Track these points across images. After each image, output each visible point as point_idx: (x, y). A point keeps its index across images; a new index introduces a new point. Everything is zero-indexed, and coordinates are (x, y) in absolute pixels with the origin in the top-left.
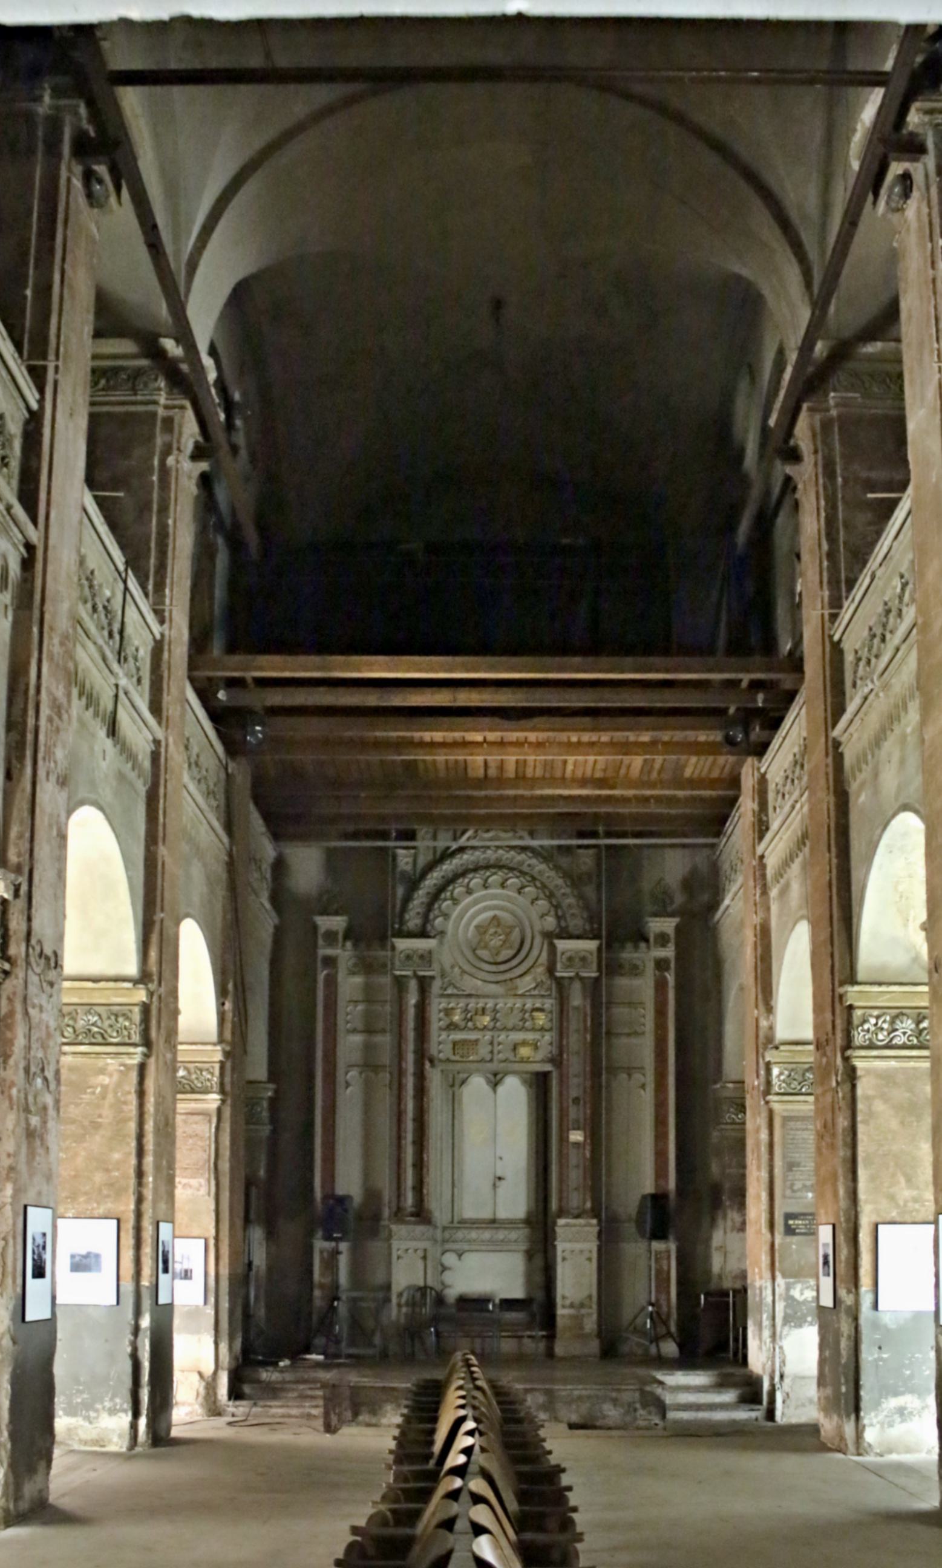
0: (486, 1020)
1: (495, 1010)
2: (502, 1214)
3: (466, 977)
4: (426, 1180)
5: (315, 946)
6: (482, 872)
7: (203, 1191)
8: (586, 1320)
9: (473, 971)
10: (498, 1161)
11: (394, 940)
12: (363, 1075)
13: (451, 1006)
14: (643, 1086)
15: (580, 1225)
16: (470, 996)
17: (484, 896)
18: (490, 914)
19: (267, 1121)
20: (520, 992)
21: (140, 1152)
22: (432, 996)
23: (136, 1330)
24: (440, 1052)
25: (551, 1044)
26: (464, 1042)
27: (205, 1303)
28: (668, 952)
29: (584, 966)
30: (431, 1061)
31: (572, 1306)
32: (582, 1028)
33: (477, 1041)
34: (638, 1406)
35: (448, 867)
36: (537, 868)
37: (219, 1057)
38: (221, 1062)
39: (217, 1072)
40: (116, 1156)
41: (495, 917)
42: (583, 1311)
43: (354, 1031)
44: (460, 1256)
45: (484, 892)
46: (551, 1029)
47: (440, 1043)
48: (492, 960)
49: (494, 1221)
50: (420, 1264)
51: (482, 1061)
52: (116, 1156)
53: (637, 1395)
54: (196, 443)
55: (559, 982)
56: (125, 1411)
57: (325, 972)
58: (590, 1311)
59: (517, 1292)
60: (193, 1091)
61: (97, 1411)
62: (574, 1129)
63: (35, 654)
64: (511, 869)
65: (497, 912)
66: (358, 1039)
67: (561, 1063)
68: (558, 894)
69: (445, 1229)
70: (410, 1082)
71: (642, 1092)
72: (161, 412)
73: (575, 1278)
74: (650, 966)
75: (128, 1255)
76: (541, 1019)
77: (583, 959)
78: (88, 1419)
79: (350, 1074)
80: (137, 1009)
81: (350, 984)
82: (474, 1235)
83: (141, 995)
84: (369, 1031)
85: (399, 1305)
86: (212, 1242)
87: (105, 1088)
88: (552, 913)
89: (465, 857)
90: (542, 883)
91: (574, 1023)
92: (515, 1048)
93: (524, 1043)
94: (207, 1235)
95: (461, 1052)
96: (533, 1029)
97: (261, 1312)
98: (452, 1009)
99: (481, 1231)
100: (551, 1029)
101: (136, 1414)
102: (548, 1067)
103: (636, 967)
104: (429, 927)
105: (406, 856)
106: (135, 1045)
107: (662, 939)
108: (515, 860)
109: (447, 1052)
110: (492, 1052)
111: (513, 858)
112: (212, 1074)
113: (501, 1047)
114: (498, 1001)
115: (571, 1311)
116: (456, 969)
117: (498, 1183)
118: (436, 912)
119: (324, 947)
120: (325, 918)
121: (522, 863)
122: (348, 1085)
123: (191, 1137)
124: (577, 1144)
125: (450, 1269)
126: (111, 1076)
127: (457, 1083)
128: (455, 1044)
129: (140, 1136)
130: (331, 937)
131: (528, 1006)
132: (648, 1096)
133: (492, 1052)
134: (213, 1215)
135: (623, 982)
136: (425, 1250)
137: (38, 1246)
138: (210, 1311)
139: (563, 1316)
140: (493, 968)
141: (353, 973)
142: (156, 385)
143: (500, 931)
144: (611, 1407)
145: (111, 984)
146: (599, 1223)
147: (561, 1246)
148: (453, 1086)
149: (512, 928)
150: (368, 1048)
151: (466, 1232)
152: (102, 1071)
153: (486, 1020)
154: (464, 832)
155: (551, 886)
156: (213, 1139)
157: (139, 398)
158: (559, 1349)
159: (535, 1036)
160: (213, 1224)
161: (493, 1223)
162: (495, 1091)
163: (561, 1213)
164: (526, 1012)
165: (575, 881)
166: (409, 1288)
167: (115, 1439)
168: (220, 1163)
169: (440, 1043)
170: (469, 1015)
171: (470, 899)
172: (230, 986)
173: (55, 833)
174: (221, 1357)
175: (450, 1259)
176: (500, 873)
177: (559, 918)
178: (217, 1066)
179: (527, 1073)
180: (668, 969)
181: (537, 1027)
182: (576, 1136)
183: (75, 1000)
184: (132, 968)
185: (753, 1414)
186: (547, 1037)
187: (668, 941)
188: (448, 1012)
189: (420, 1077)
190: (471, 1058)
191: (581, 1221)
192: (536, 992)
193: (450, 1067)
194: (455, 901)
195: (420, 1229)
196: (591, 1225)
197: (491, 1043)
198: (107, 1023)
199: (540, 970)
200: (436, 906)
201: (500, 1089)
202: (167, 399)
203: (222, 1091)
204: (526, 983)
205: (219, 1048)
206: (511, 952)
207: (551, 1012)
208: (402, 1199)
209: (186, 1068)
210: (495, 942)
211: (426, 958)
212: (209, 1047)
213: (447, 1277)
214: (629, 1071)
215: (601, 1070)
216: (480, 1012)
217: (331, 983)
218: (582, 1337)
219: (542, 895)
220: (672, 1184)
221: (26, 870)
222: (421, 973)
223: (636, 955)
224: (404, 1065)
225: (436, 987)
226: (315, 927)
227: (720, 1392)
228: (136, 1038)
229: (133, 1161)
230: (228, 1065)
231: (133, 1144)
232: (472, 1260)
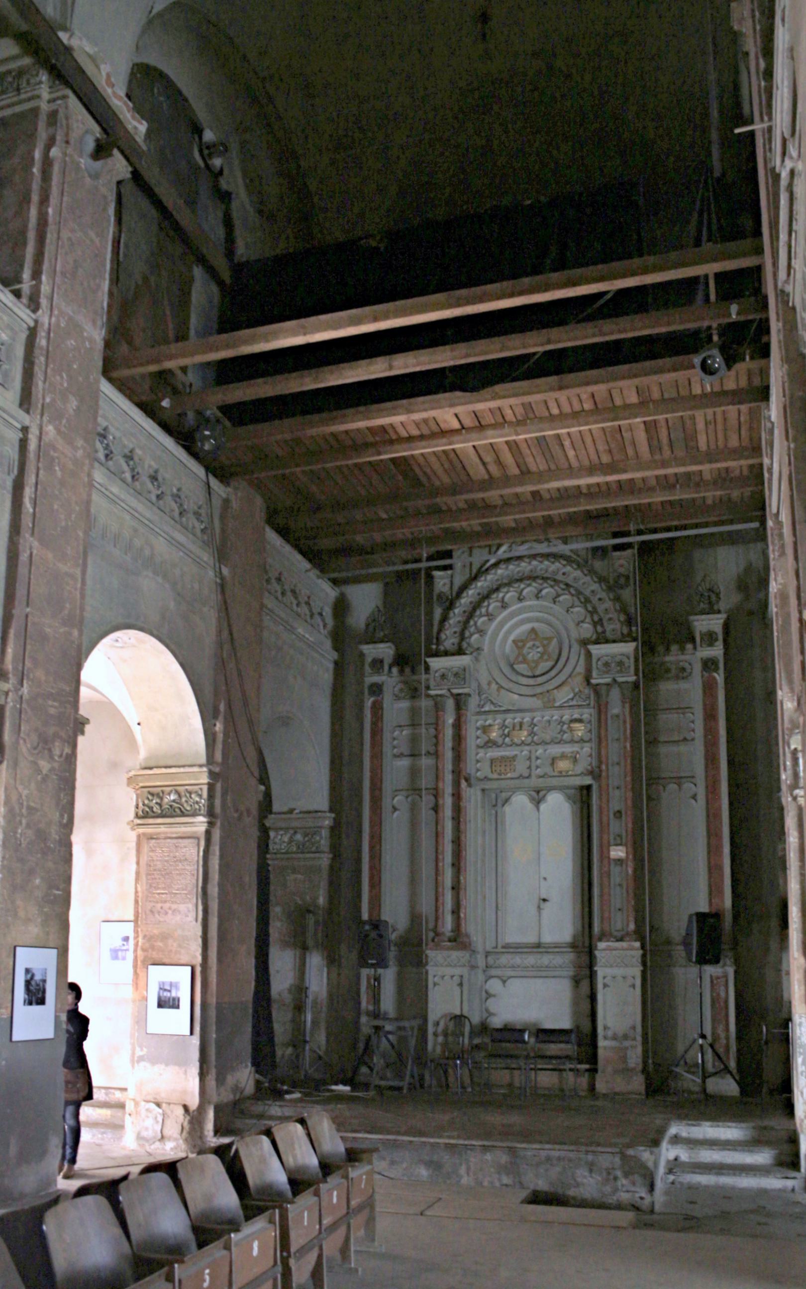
0: (524, 735)
1: (533, 724)
2: (547, 939)
3: (503, 691)
4: (463, 903)
5: (363, 675)
6: (516, 585)
8: (629, 1053)
9: (511, 685)
10: (543, 882)
11: (428, 660)
12: (410, 799)
13: (487, 723)
14: (694, 797)
15: (623, 949)
16: (508, 711)
17: (520, 608)
18: (527, 627)
19: (327, 849)
20: (557, 704)
22: (469, 714)
24: (478, 770)
25: (591, 756)
26: (503, 759)
27: (192, 1033)
28: (717, 651)
29: (621, 671)
30: (467, 780)
31: (615, 1038)
32: (622, 737)
33: (514, 758)
34: (619, 1173)
35: (482, 584)
36: (572, 576)
37: (205, 779)
38: (209, 784)
39: (205, 794)
41: (533, 630)
42: (627, 1044)
43: (401, 755)
44: (504, 982)
45: (519, 605)
46: (590, 741)
47: (478, 761)
48: (530, 674)
49: (538, 945)
50: (457, 990)
51: (521, 777)
53: (617, 1160)
54: (97, 140)
55: (596, 689)
57: (372, 699)
58: (634, 1043)
59: (565, 1023)
60: (183, 815)
62: (617, 845)
64: (545, 579)
65: (536, 625)
66: (405, 762)
67: (600, 776)
68: (595, 600)
69: (487, 954)
70: (448, 802)
71: (693, 801)
72: (45, 107)
73: (619, 1008)
74: (698, 667)
76: (580, 730)
77: (620, 664)
79: (396, 799)
81: (396, 709)
82: (518, 960)
84: (414, 755)
85: (435, 1034)
86: (198, 970)
88: (588, 619)
89: (500, 572)
90: (576, 590)
91: (613, 731)
92: (553, 761)
93: (563, 756)
94: (194, 962)
95: (498, 769)
96: (572, 741)
97: (321, 1039)
98: (490, 725)
99: (524, 956)
100: (590, 741)
102: (588, 781)
103: (683, 669)
104: (464, 645)
105: (442, 578)
107: (710, 638)
108: (551, 569)
109: (485, 771)
110: (529, 768)
111: (548, 567)
112: (200, 796)
113: (539, 761)
114: (535, 714)
115: (613, 1043)
116: (494, 686)
117: (543, 905)
118: (472, 629)
119: (371, 675)
120: (371, 646)
121: (555, 573)
122: (395, 809)
123: (180, 861)
124: (619, 861)
125: (494, 996)
127: (500, 803)
128: (492, 761)
130: (377, 664)
131: (566, 718)
132: (699, 808)
133: (529, 768)
134: (200, 941)
135: (666, 687)
136: (462, 976)
138: (196, 1041)
139: (605, 1048)
140: (531, 681)
141: (397, 698)
142: (38, 79)
143: (537, 643)
144: (586, 1174)
146: (643, 947)
147: (601, 972)
148: (495, 806)
149: (550, 639)
150: (414, 773)
151: (509, 956)
153: (524, 735)
154: (499, 546)
155: (587, 593)
156: (201, 863)
157: (23, 96)
158: (601, 1086)
159: (576, 748)
160: (200, 950)
161: (538, 947)
162: (538, 809)
163: (603, 936)
164: (564, 723)
165: (613, 585)
166: (445, 1016)
168: (209, 887)
169: (478, 761)
170: (506, 731)
171: (505, 613)
172: (222, 707)
175: (494, 985)
176: (534, 584)
177: (595, 624)
178: (205, 788)
179: (568, 787)
180: (716, 669)
181: (576, 738)
182: (618, 853)
185: (790, 1183)
186: (587, 749)
187: (716, 640)
188: (486, 729)
189: (457, 796)
190: (509, 775)
191: (624, 944)
192: (574, 703)
193: (487, 785)
194: (491, 617)
195: (455, 954)
196: (632, 949)
197: (529, 759)
199: (579, 680)
200: (472, 623)
201: (543, 807)
202: (50, 93)
203: (211, 813)
204: (563, 696)
205: (205, 769)
206: (550, 664)
207: (590, 722)
208: (440, 922)
209: (177, 792)
210: (533, 655)
211: (461, 675)
212: (196, 769)
213: (491, 1004)
214: (679, 780)
215: (648, 784)
216: (518, 727)
217: (377, 709)
218: (627, 1071)
219: (577, 603)
220: (728, 902)
222: (455, 691)
223: (682, 657)
224: (440, 785)
225: (473, 703)
226: (362, 655)
227: (751, 1151)
230: (219, 786)
232: (515, 985)
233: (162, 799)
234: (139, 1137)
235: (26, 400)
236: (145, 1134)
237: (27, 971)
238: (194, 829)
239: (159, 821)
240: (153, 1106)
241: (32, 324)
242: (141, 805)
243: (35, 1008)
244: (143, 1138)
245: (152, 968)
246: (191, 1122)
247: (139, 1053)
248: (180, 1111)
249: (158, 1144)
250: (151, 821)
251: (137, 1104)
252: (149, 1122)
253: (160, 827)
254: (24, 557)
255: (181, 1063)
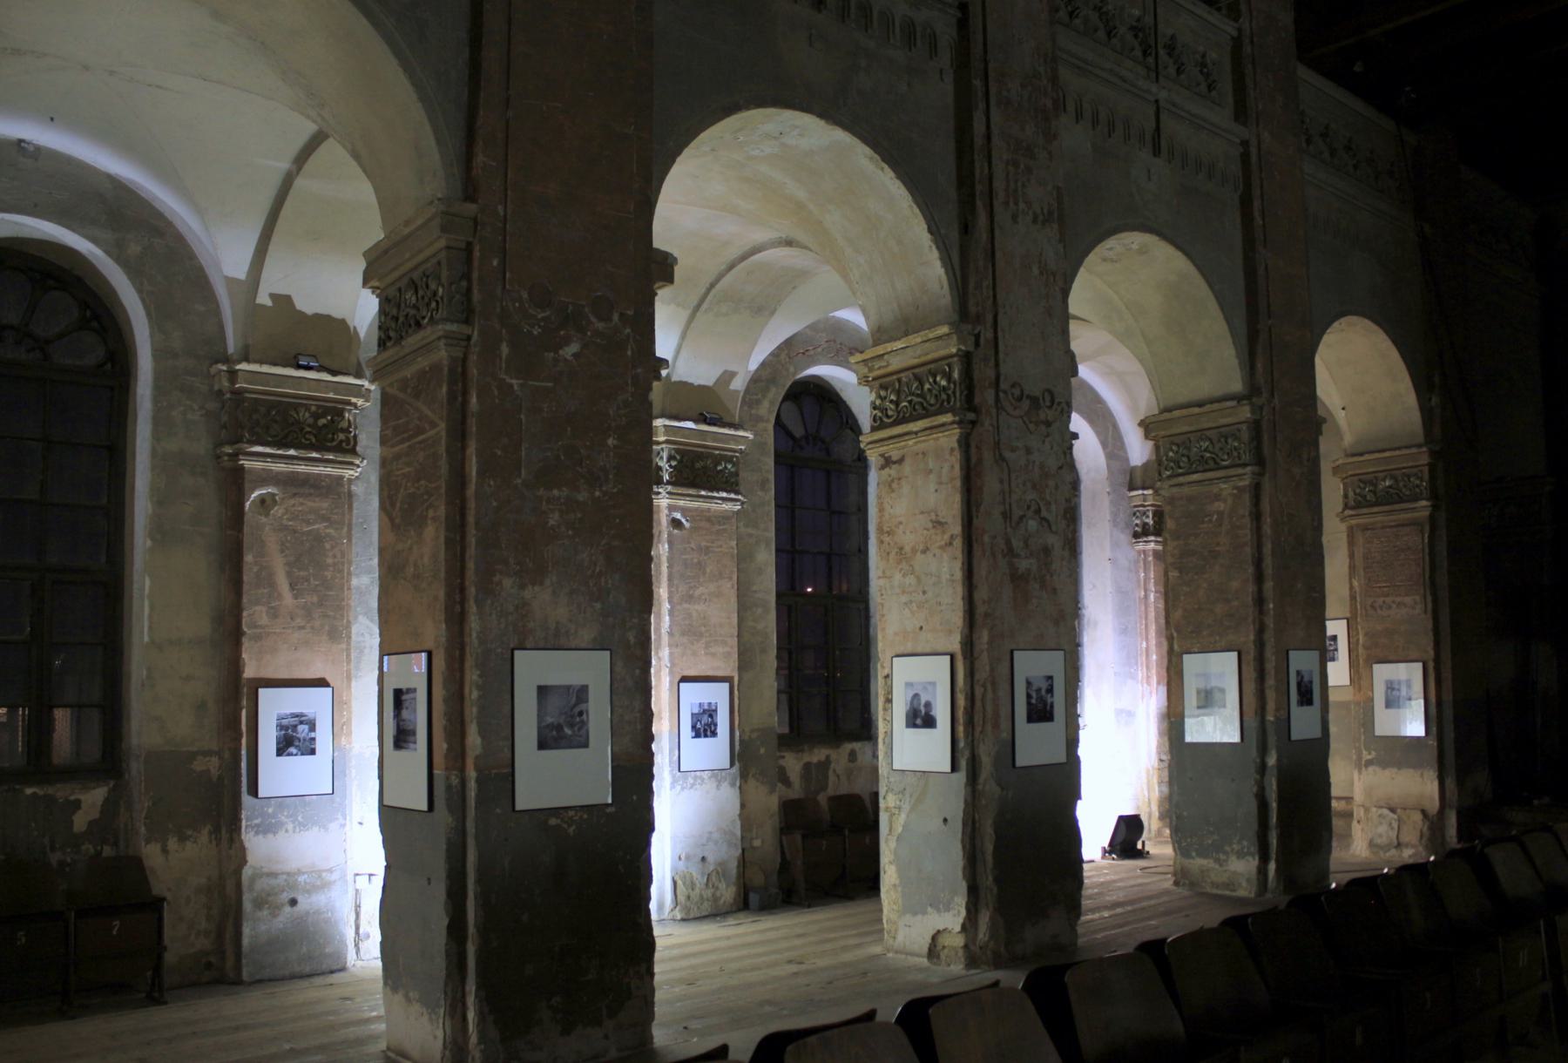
7: (1419, 609)
21: (1259, 578)
23: (1262, 768)
27: (954, 768)
39: (1426, 476)
40: (1235, 584)
52: (1235, 584)
56: (1252, 855)
60: (1401, 501)
61: (1226, 853)
63: (982, 106)
75: (1250, 687)
78: (1217, 861)
80: (1244, 427)
83: (1245, 412)
86: (1431, 665)
87: (1220, 514)
101: (1264, 859)
106: (1245, 465)
126: (1225, 501)
129: (1258, 563)
137: (1039, 690)
145: (1216, 406)
152: (1217, 497)
167: (1244, 884)
172: (1437, 379)
173: (1036, 271)
174: (1448, 794)
178: (1426, 469)
183: (1185, 429)
184: (1237, 386)
198: (1218, 446)
203: (1434, 496)
212: (1414, 450)
221: (989, 318)
228: (1246, 458)
229: (1251, 588)
231: (1251, 570)
233: (1376, 486)
234: (1372, 844)
235: (1241, 112)
236: (1379, 841)
237: (1298, 673)
238: (1416, 515)
239: (1375, 509)
240: (1386, 811)
241: (1235, 33)
242: (1351, 494)
243: (1305, 708)
244: (1377, 846)
245: (1376, 667)
246: (1431, 828)
247: (1366, 756)
248: (1418, 817)
249: (1393, 852)
250: (1365, 511)
251: (1367, 810)
252: (1383, 829)
253: (1377, 516)
254: (1261, 271)
255: (1418, 765)
